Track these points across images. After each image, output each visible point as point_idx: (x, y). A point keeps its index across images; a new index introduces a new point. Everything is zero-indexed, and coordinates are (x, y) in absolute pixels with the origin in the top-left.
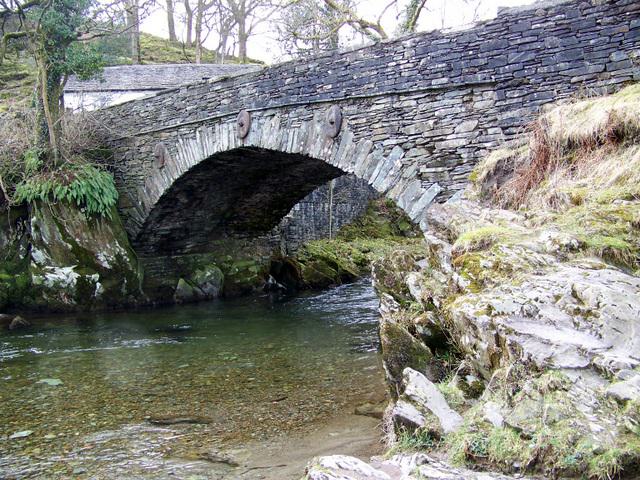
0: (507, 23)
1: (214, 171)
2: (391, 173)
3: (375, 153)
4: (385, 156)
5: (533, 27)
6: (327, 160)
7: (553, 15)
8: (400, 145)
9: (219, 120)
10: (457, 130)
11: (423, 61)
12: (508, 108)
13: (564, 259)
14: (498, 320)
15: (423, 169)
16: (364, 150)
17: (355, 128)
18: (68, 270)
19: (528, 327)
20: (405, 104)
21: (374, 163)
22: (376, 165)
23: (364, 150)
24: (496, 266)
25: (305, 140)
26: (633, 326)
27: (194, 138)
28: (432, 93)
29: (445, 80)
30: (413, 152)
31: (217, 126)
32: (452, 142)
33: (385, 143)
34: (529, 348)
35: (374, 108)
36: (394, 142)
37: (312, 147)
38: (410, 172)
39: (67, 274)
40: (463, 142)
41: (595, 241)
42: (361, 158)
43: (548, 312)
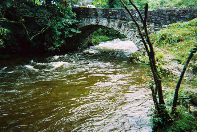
3: (128, 31)
7: (168, 12)
9: (91, 18)
12: (156, 27)
13: (173, 61)
14: (169, 70)
16: (126, 30)
17: (125, 26)
19: (172, 71)
21: (128, 33)
23: (126, 30)
24: (165, 61)
25: (114, 26)
27: (84, 20)
30: (136, 32)
31: (91, 19)
33: (131, 29)
34: (174, 73)
35: (129, 22)
36: (133, 30)
38: (135, 36)
41: (176, 58)
42: (125, 32)
43: (175, 69)
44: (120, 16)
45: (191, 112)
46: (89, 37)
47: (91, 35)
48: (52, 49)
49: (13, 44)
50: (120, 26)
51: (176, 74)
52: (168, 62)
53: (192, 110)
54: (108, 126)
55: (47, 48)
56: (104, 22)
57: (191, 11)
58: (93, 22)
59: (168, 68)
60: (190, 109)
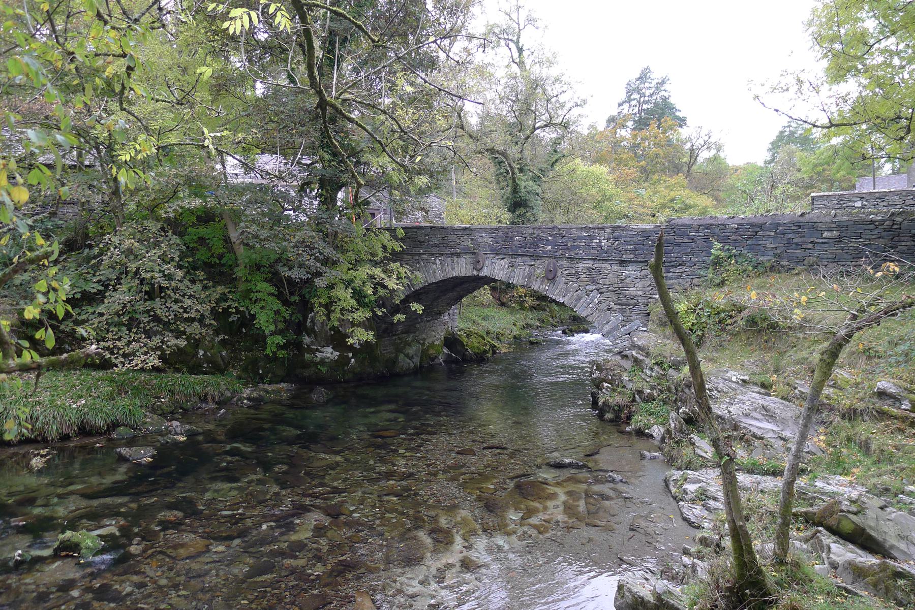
0: (777, 137)
1: (274, 244)
2: (591, 306)
4: (588, 295)
5: (691, 234)
6: (750, 532)
8: (598, 290)
9: (458, 255)
10: (636, 285)
11: (616, 243)
15: (612, 305)
18: (330, 349)
19: (744, 420)
20: (603, 266)
22: (580, 300)
26: (107, 74)
28: (622, 263)
29: (632, 256)
31: (455, 259)
32: (632, 291)
33: (587, 287)
37: (534, 283)
38: (604, 306)
39: (329, 353)
40: (640, 293)
43: (754, 414)
44: (550, 247)
45: (834, 566)
46: (449, 314)
47: (454, 310)
48: (329, 355)
49: (285, 272)
50: (551, 277)
51: (759, 433)
52: (725, 390)
53: (839, 560)
54: (796, 274)
55: (314, 352)
56: (497, 268)
57: (900, 118)
58: (462, 268)
59: (729, 412)
60: (831, 556)
